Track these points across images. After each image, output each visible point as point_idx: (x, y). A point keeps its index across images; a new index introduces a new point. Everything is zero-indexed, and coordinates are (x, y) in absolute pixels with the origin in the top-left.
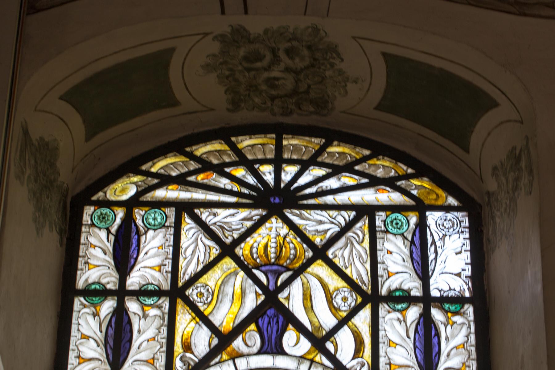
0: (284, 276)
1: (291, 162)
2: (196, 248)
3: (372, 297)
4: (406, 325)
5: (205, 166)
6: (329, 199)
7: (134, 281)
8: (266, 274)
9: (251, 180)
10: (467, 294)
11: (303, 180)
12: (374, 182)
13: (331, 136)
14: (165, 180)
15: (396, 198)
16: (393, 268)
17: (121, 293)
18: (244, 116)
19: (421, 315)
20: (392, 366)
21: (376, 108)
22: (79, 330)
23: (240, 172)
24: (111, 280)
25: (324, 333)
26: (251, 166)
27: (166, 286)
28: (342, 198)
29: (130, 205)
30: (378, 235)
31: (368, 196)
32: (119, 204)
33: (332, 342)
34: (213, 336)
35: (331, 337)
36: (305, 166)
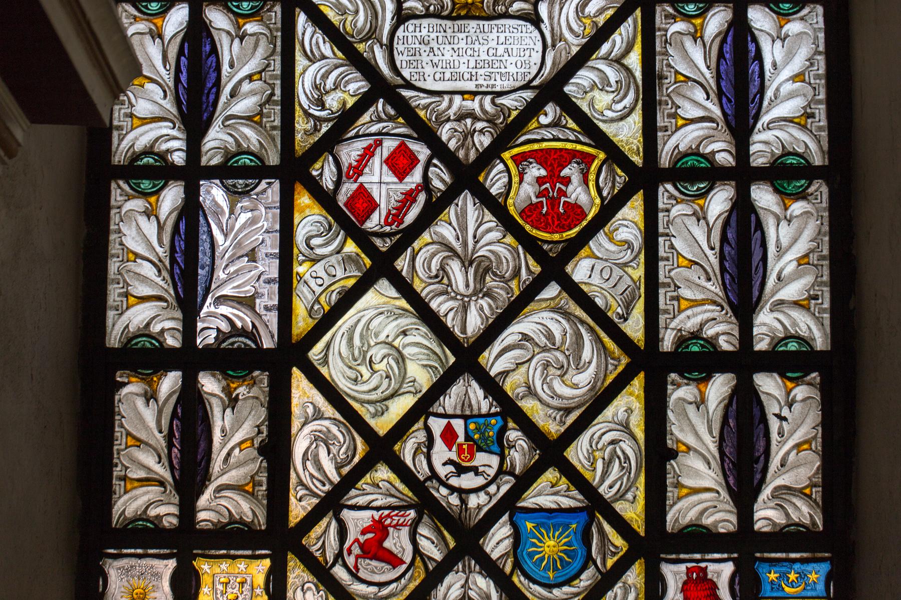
4: (708, 225)
10: (817, 160)
19: (731, 24)
20: (682, 301)
22: (121, 244)
27: (273, 159)
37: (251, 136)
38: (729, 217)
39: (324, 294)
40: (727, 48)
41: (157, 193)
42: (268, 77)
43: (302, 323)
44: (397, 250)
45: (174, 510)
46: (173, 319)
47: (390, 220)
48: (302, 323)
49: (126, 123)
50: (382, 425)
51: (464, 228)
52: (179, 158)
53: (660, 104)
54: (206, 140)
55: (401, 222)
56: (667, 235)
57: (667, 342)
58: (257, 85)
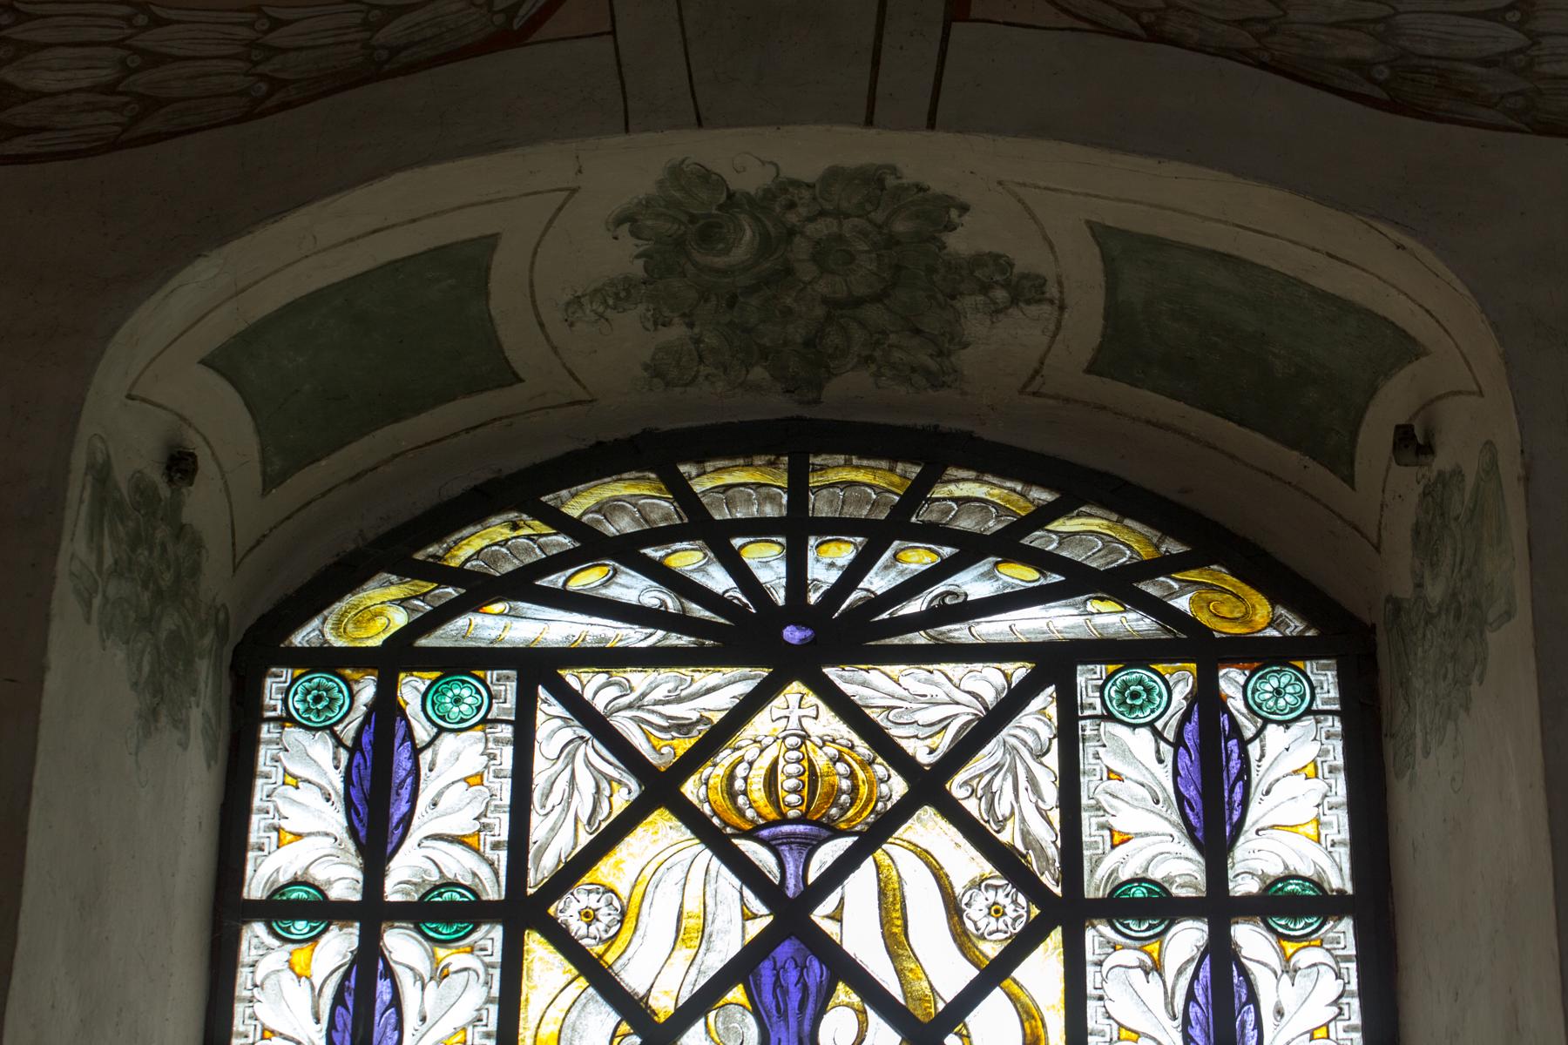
0: (828, 854)
1: (836, 528)
2: (575, 788)
3: (1065, 906)
5: (592, 545)
6: (959, 633)
7: (406, 872)
8: (771, 845)
9: (719, 581)
11: (877, 582)
12: (1077, 582)
13: (936, 452)
14: (480, 590)
15: (1138, 624)
16: (1126, 819)
17: (1218, 907)
18: (713, 398)
21: (1088, 371)
22: (254, 1017)
23: (687, 558)
24: (342, 879)
25: (941, 1006)
26: (719, 540)
27: (493, 891)
28: (991, 628)
29: (396, 657)
30: (1087, 727)
31: (1056, 621)
32: (359, 658)
33: (960, 1035)
34: (625, 1028)
35: (630, 1023)
36: (876, 538)
37: (458, 864)
41: (314, 939)
53: (1084, 741)
56: (1101, 998)
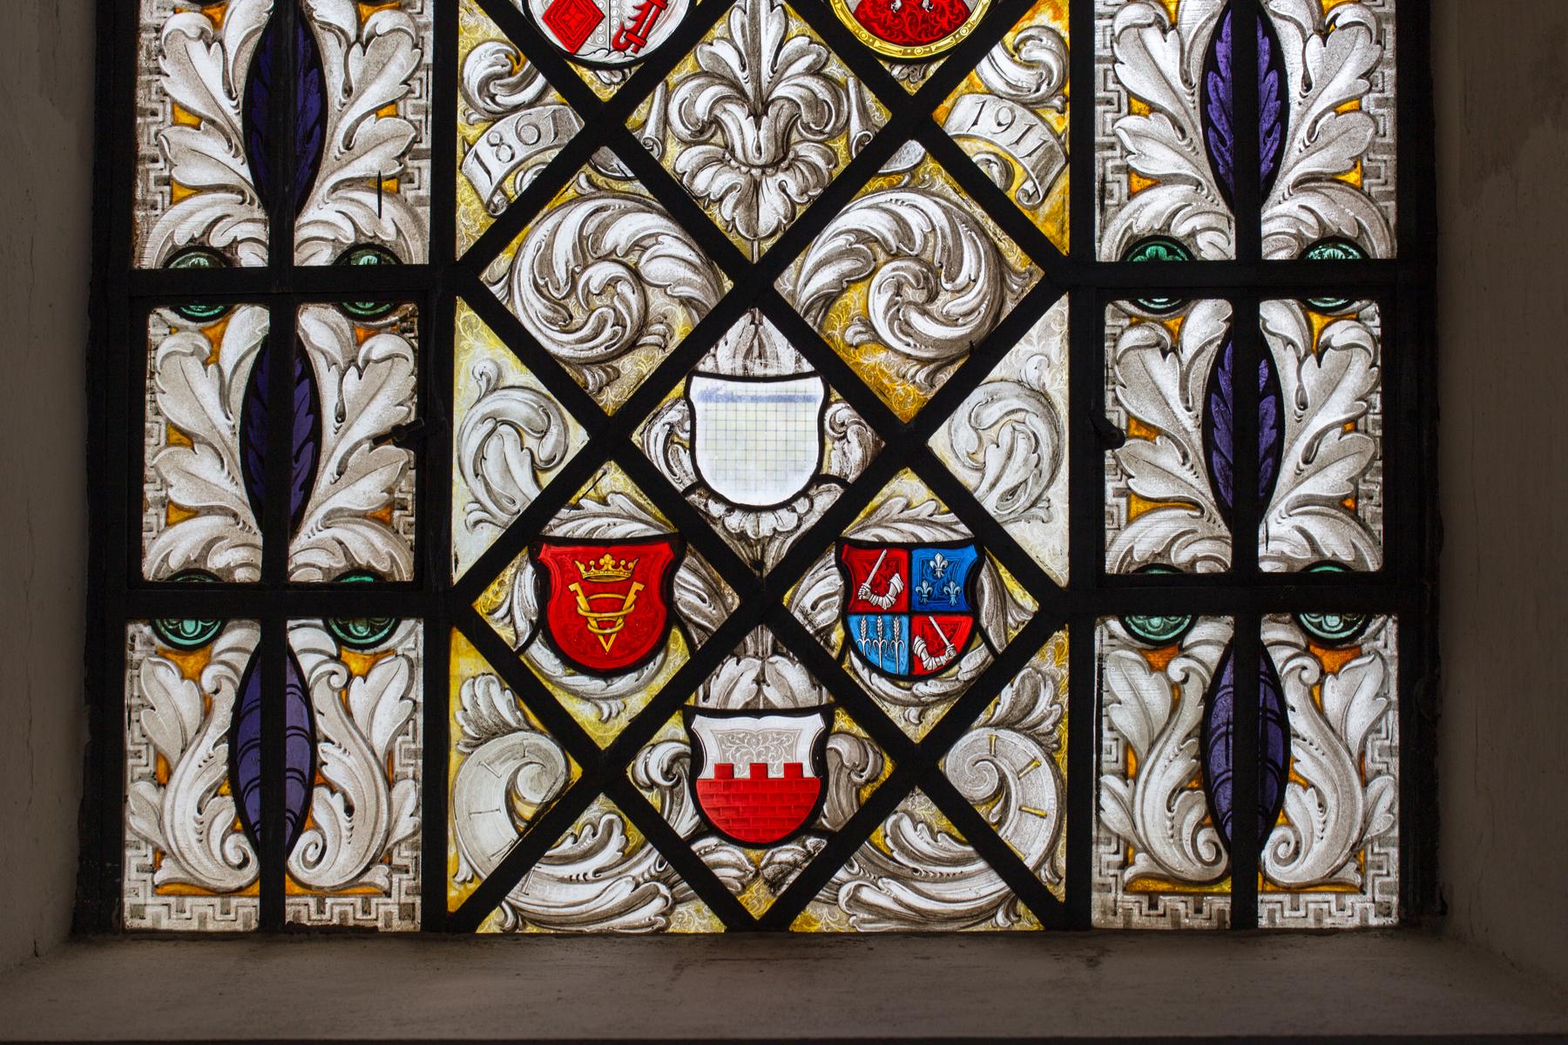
38: (1222, 348)
39: (512, 177)
40: (1222, 49)
42: (409, 109)
43: (470, 224)
44: (634, 92)
45: (260, 231)
46: (253, 221)
47: (622, 40)
48: (470, 224)
49: (159, 195)
50: (611, 399)
51: (755, 49)
52: (252, 257)
54: (303, 219)
55: (642, 42)
57: (1107, 249)
58: (388, 125)
